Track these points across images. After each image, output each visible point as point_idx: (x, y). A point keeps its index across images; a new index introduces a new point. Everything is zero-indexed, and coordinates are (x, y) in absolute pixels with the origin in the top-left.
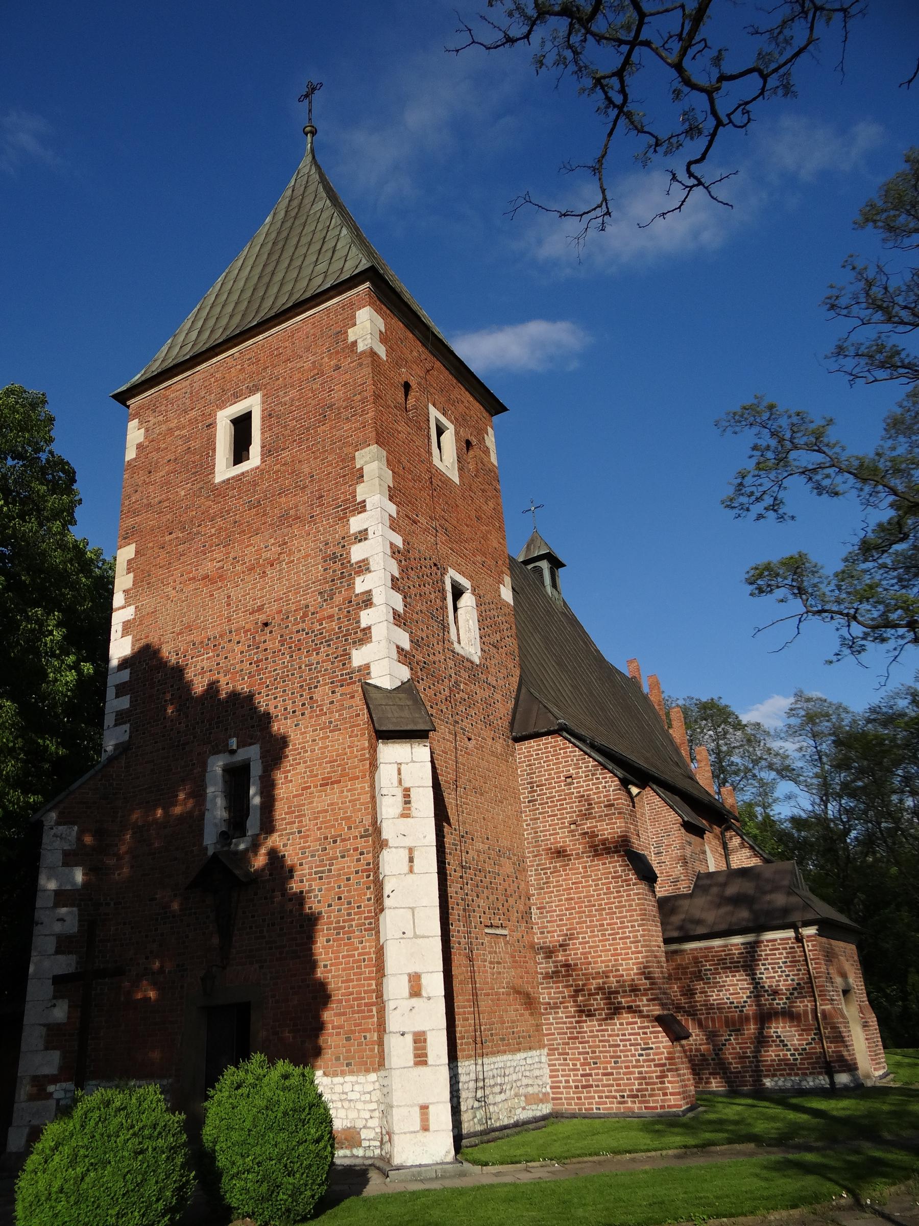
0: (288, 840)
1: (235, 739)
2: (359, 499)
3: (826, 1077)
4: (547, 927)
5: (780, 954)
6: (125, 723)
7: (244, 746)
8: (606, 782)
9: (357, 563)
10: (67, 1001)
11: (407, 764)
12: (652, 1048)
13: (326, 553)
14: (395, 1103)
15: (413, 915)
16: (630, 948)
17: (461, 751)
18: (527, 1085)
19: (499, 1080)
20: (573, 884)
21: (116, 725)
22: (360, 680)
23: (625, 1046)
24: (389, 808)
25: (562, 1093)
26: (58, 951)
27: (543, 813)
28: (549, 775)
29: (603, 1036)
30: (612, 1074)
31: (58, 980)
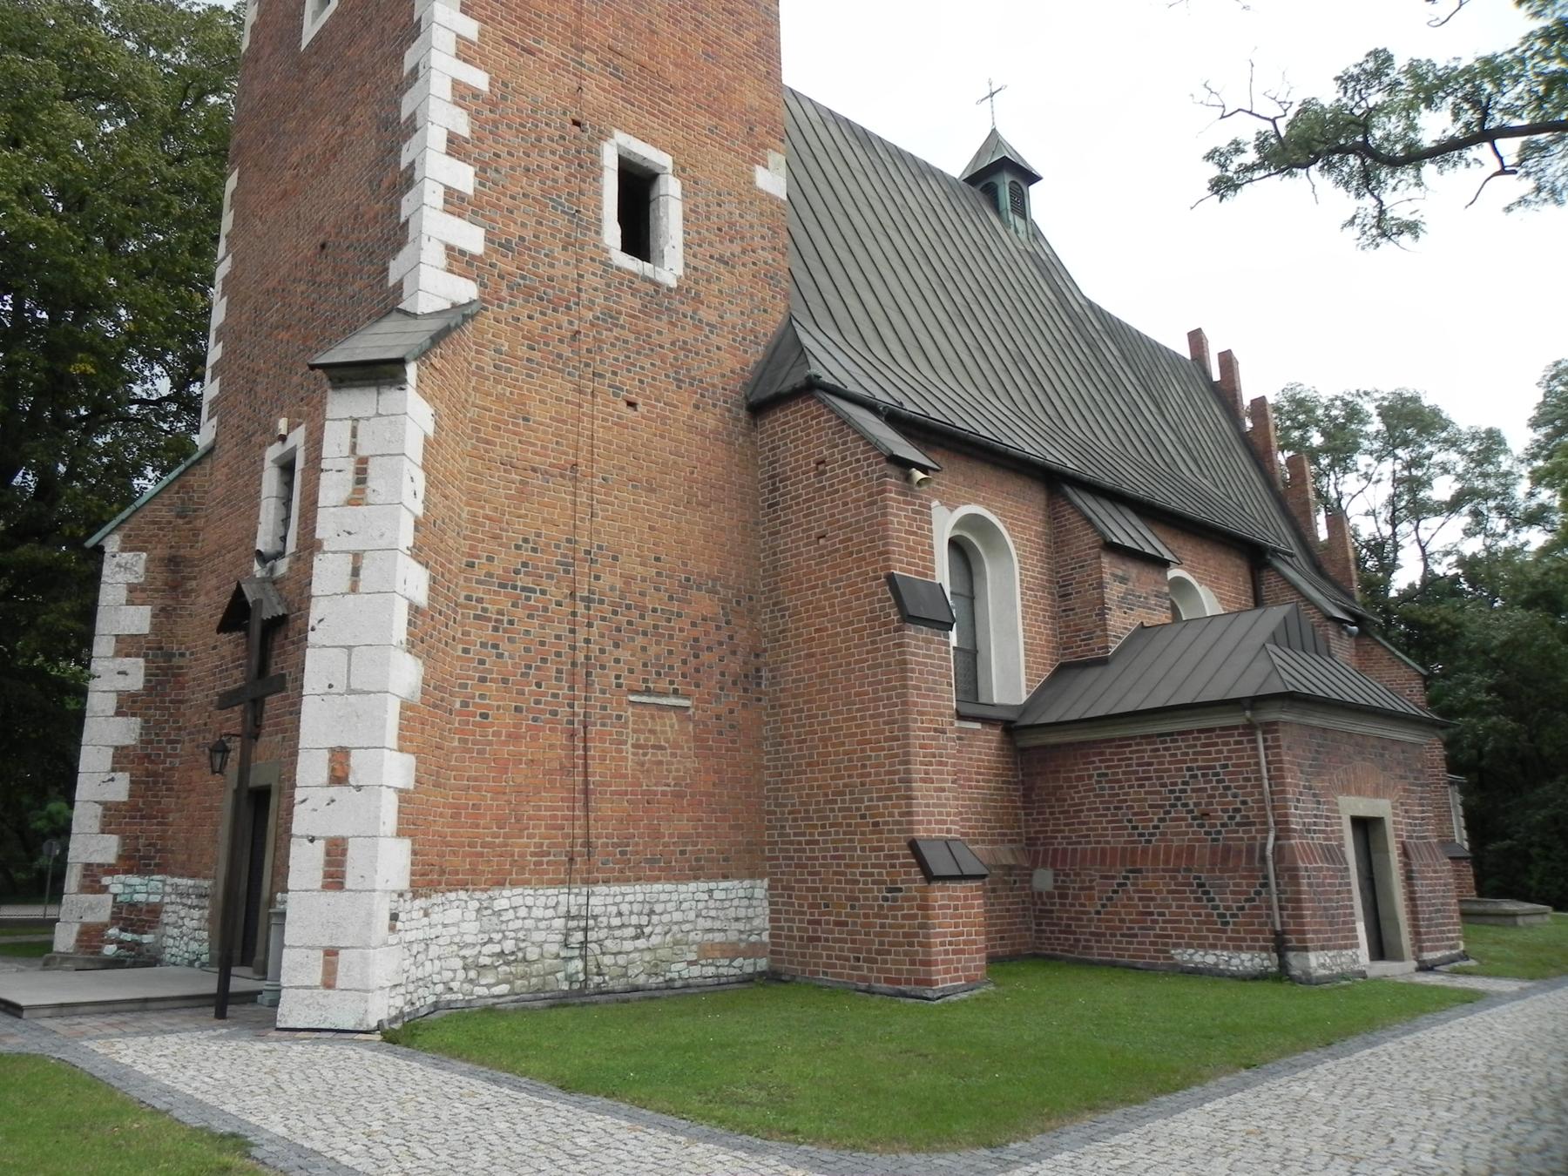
3: (1274, 955)
5: (1218, 752)
11: (368, 419)
23: (866, 883)
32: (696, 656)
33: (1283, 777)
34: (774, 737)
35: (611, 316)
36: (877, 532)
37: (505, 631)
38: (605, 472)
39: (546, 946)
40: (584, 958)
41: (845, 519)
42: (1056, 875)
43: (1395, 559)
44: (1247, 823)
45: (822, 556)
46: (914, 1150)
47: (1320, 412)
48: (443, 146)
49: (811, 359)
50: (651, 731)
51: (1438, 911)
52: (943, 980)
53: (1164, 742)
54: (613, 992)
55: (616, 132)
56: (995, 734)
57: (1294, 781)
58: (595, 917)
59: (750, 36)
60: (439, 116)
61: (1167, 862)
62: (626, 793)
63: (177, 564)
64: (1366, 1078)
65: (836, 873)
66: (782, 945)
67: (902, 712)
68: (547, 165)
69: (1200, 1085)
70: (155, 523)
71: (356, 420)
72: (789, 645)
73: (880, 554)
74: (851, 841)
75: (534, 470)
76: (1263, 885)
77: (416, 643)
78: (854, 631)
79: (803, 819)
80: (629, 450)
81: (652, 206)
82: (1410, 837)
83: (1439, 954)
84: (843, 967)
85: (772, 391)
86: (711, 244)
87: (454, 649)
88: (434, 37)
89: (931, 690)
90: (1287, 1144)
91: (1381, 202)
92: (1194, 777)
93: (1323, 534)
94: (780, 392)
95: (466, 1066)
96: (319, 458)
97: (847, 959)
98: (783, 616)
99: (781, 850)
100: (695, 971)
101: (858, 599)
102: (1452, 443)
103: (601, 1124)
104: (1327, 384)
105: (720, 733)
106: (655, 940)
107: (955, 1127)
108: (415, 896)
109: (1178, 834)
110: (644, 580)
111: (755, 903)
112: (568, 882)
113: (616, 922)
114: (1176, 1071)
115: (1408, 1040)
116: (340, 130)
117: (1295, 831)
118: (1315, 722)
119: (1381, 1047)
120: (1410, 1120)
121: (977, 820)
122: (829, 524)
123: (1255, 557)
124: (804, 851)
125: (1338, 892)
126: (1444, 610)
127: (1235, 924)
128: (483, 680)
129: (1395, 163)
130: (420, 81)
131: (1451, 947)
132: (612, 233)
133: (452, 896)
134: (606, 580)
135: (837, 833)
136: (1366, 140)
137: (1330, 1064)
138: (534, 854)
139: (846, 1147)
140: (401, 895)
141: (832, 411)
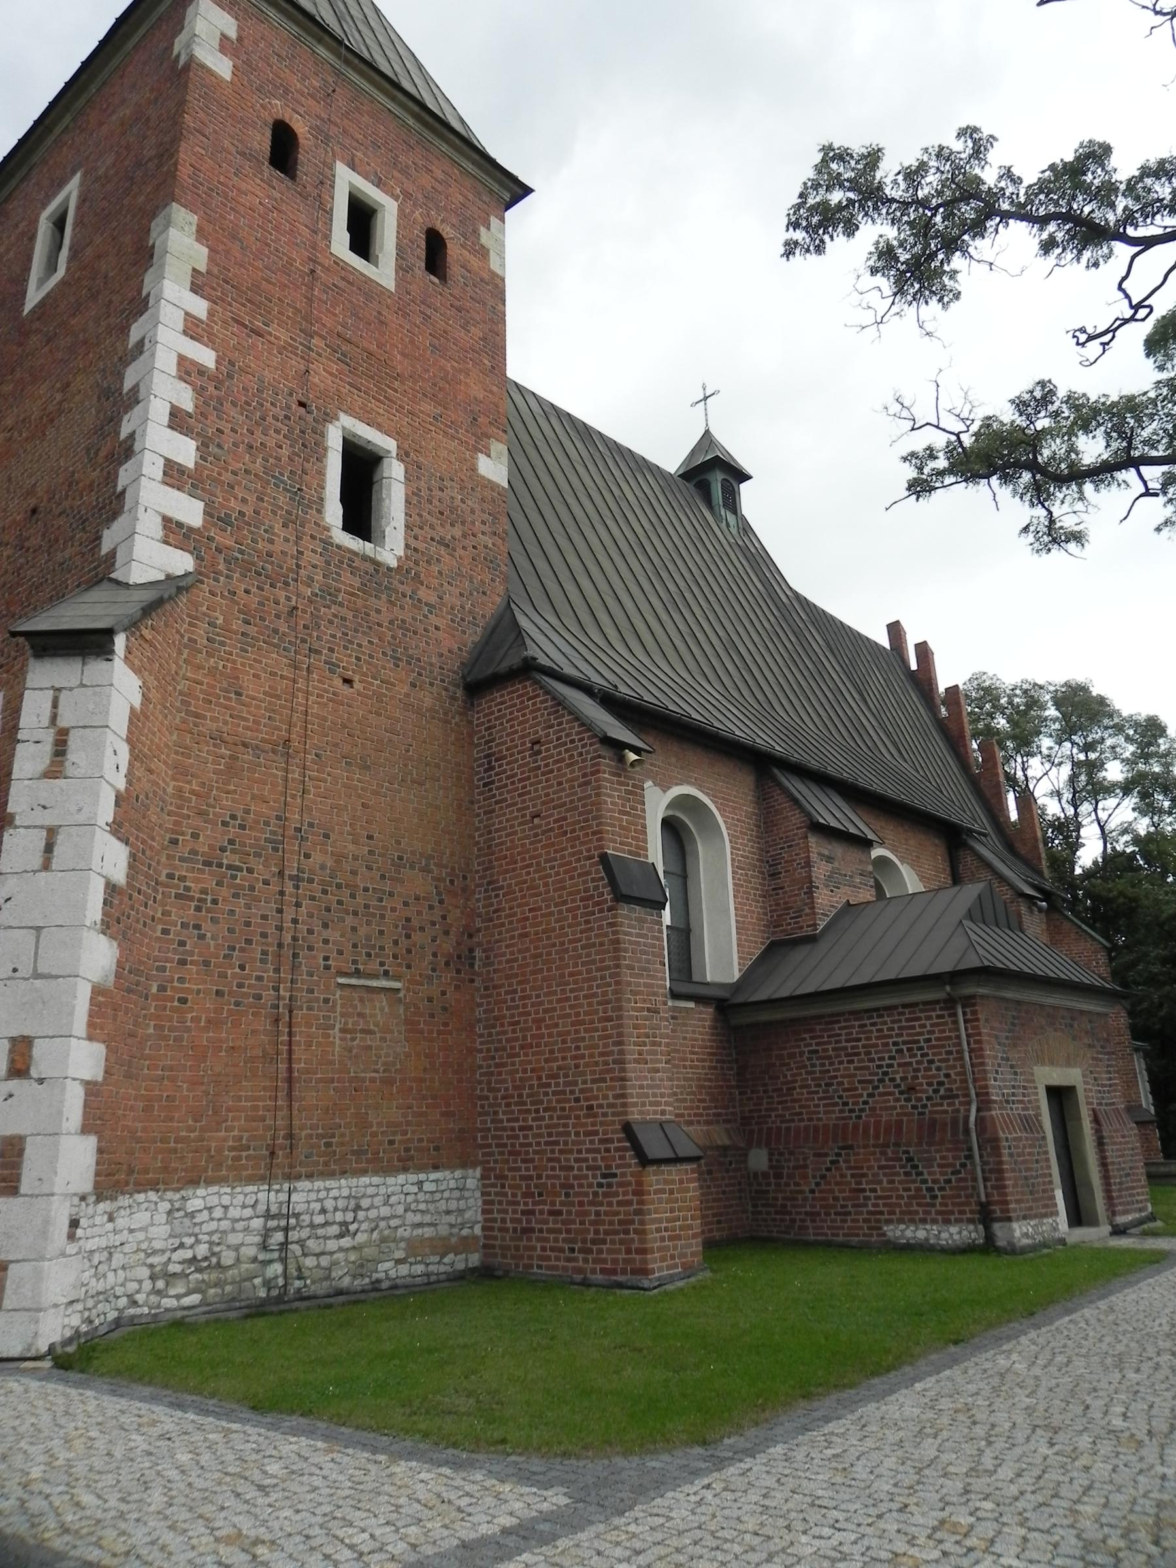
3: (981, 1227)
11: (71, 689)
32: (408, 936)
33: (982, 1049)
34: (487, 1019)
35: (329, 594)
36: (591, 812)
37: (208, 911)
38: (320, 748)
39: (243, 1250)
40: (284, 1261)
41: (560, 798)
42: (771, 1154)
43: (1078, 837)
44: (950, 1096)
45: (536, 835)
46: (626, 1454)
47: (1003, 701)
48: (165, 419)
49: (528, 641)
50: (360, 1015)
51: (1128, 1175)
52: (660, 1269)
53: (872, 1017)
54: (315, 1297)
55: (342, 415)
56: (708, 1012)
57: (992, 1053)
58: (297, 1216)
59: (477, 332)
60: (164, 390)
61: (877, 1137)
62: (332, 1080)
64: (1065, 1346)
65: (550, 1160)
66: (495, 1238)
67: (616, 992)
68: (271, 443)
69: (911, 1364)
71: (59, 690)
72: (503, 925)
73: (594, 833)
74: (566, 1125)
75: (245, 745)
76: (967, 1157)
77: (111, 924)
78: (568, 910)
79: (516, 1104)
80: (344, 726)
81: (375, 487)
82: (1100, 1104)
83: (1130, 1217)
84: (558, 1259)
85: (490, 671)
86: (432, 527)
87: (154, 931)
88: (162, 312)
89: (645, 969)
90: (992, 1419)
91: (1050, 513)
92: (900, 1051)
93: (1014, 816)
94: (496, 671)
95: (147, 1391)
96: (16, 728)
98: (497, 896)
99: (494, 1137)
100: (404, 1270)
102: (1119, 729)
103: (295, 1447)
104: (1010, 674)
105: (432, 1016)
106: (361, 1238)
107: (670, 1426)
108: (100, 1199)
109: (886, 1109)
110: (355, 858)
111: (467, 1194)
112: (267, 1178)
113: (319, 1219)
114: (888, 1351)
115: (1103, 1305)
116: (59, 396)
117: (995, 1102)
118: (1009, 995)
119: (1079, 1314)
120: (1103, 1385)
121: (692, 1101)
122: (544, 803)
123: (952, 838)
124: (517, 1137)
125: (1037, 1161)
126: (1121, 884)
127: (943, 1197)
128: (182, 962)
129: (1062, 480)
130: (146, 355)
131: (1140, 1210)
132: (334, 512)
133: (141, 1197)
134: (317, 858)
136: (1035, 458)
137: (1033, 1334)
138: (231, 1149)
139: (556, 1455)
140: (83, 1198)
141: (547, 693)
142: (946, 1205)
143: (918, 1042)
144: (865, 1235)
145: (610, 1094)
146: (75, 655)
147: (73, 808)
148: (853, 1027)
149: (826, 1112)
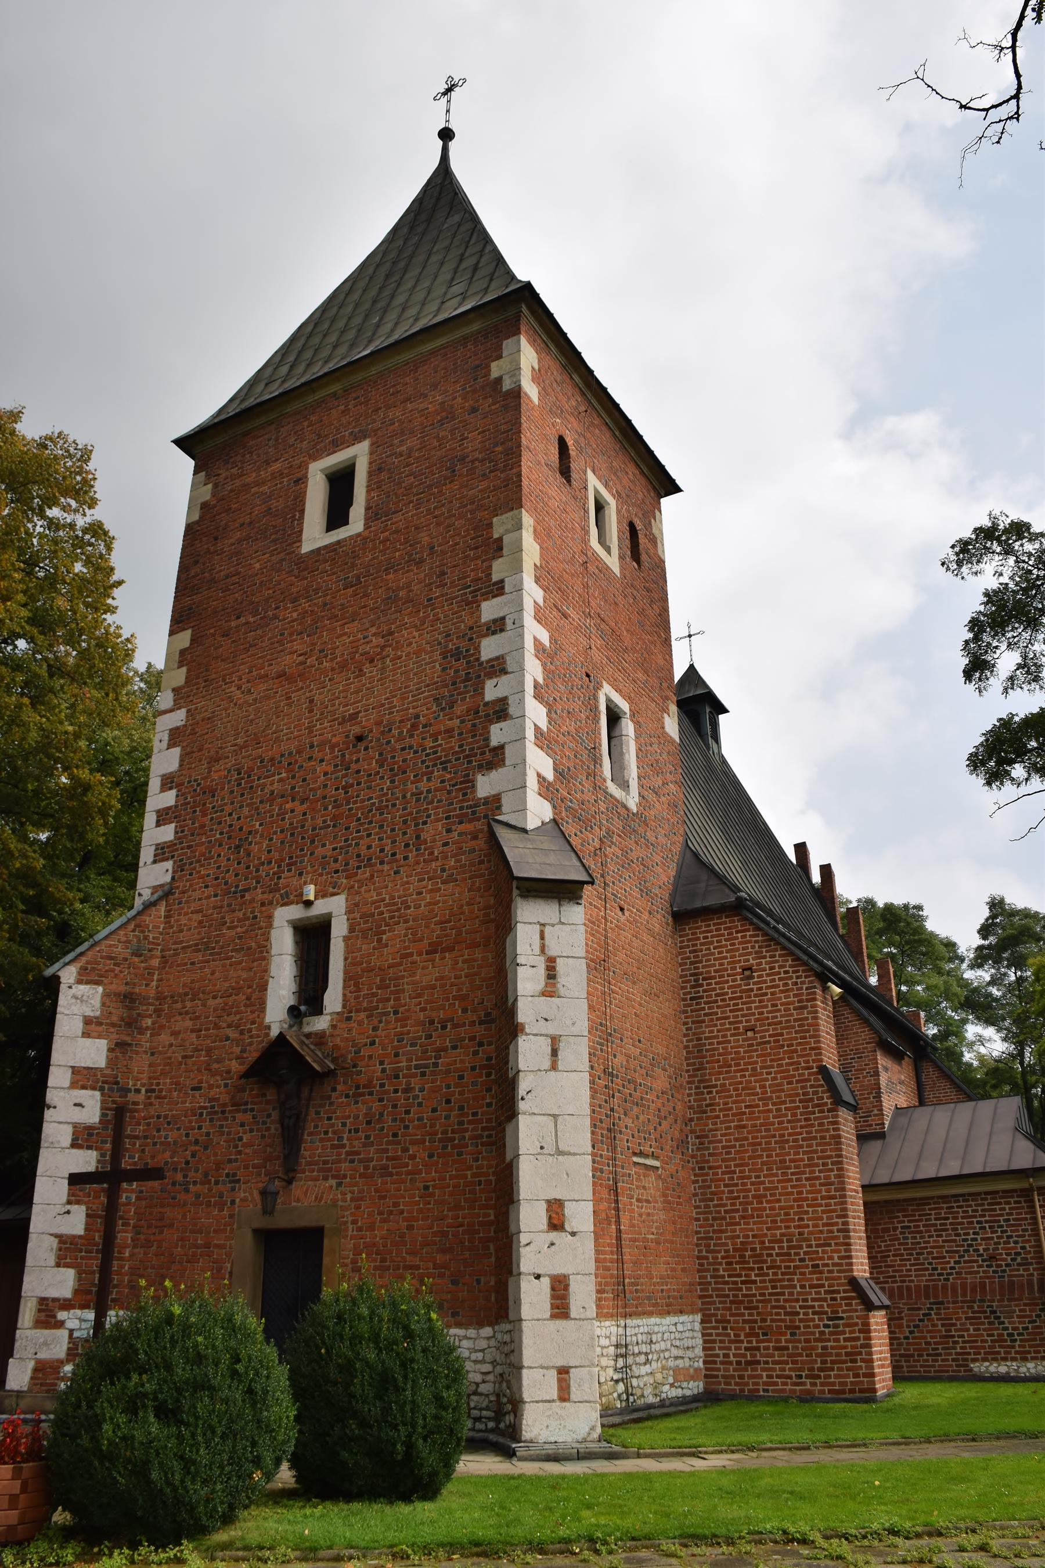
0: (380, 1022)
1: (312, 887)
2: (495, 578)
4: (708, 1161)
6: (167, 859)
7: (324, 896)
8: (797, 977)
9: (488, 661)
10: (83, 1208)
11: (553, 925)
12: (842, 1318)
13: (446, 647)
14: (525, 1364)
15: (556, 1126)
16: (820, 1191)
17: (611, 922)
18: (676, 1358)
19: (644, 1348)
20: (746, 1107)
21: (155, 862)
22: (486, 817)
24: (527, 981)
25: (719, 1370)
26: (74, 1145)
27: (711, 1014)
28: (721, 964)
29: (778, 1301)
30: (787, 1348)
31: (75, 1179)
61: (964, 1294)
63: (133, 1001)
70: (111, 958)
72: (718, 1117)
97: (790, 1377)
98: (709, 1093)
101: (789, 1083)
109: (971, 1273)
122: (757, 1020)
135: (774, 1274)
142: (1024, 1347)
143: (999, 1221)
144: (953, 1371)
145: (836, 1255)
146: (552, 898)
147: (569, 1022)
148: (942, 1208)
149: (916, 1276)
